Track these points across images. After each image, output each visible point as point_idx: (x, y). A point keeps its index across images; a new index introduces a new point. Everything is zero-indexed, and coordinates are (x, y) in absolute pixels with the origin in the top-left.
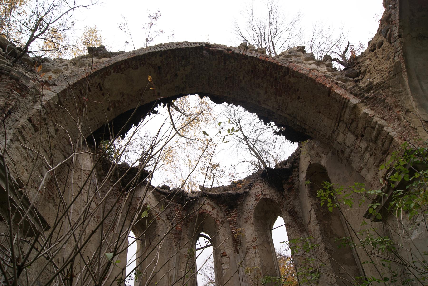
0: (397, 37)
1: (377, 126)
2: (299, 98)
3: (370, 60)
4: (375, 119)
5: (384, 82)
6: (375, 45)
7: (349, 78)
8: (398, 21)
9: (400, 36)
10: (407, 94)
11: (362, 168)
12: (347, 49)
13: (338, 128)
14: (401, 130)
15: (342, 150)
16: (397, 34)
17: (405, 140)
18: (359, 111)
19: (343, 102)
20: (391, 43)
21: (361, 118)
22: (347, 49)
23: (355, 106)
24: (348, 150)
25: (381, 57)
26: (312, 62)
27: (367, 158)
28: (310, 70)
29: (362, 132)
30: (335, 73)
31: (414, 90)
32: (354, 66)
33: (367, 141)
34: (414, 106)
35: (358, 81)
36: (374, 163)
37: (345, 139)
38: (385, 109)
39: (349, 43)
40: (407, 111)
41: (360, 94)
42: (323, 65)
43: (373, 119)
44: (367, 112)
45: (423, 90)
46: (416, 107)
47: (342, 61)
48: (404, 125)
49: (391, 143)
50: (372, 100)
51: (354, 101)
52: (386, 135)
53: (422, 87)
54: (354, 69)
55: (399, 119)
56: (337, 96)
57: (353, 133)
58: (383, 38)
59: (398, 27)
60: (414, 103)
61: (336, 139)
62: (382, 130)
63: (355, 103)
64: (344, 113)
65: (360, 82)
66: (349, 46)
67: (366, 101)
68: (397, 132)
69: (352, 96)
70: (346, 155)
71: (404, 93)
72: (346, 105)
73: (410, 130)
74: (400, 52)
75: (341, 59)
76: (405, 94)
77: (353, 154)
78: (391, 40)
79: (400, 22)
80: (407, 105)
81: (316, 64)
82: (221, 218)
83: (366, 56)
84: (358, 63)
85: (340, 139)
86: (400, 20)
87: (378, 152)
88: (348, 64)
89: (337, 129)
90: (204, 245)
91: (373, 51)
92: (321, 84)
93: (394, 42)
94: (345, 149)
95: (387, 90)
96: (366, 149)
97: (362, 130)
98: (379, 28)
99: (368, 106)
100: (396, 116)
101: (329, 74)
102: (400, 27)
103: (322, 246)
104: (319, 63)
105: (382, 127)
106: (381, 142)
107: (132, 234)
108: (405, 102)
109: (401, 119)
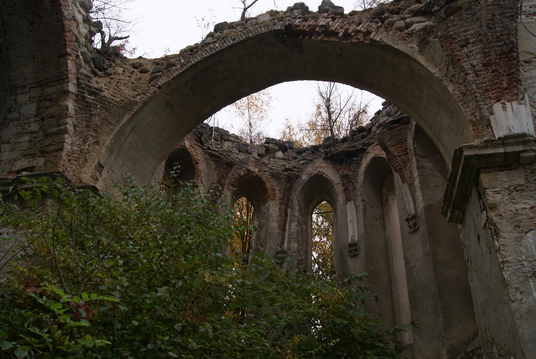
0: (157, 86)
1: (63, 127)
2: (32, 23)
3: (124, 71)
4: (69, 121)
5: (110, 102)
6: (142, 66)
7: (92, 64)
8: (172, 77)
9: (160, 88)
10: (112, 131)
11: (8, 142)
12: (121, 38)
13: (32, 89)
14: (76, 150)
15: (10, 109)
16: (160, 84)
17: (69, 160)
18: (66, 100)
19: (62, 77)
20: (150, 83)
21: (60, 105)
22: (121, 38)
23: (67, 92)
24: (16, 115)
25: (133, 80)
26: (84, 13)
27: (24, 140)
28: (73, 17)
29: (46, 116)
30: (89, 44)
31: (120, 133)
32: (110, 56)
33: (41, 127)
34: (106, 145)
35: (96, 74)
36: (24, 150)
37: (25, 104)
38: (84, 122)
39: (128, 37)
40: (97, 143)
41: (83, 88)
42: (88, 26)
43: (67, 118)
44: (70, 108)
45: (125, 140)
46: (107, 146)
47: (106, 42)
48: (82, 150)
49: (57, 151)
50: (85, 104)
51: (72, 88)
52: (60, 141)
53: (127, 137)
54: (104, 61)
55: (85, 141)
56: (64, 66)
57: (38, 108)
58: (151, 70)
59: (167, 80)
60: (109, 141)
61: (17, 95)
62: (62, 134)
63: (70, 90)
64: (53, 86)
65: (95, 76)
66: (125, 39)
67: (80, 99)
68: (71, 149)
69: (75, 82)
70: (9, 116)
71: (112, 127)
72: (62, 82)
73: (81, 158)
74: (146, 97)
75: (107, 39)
76: (111, 129)
77: (16, 123)
78: (152, 81)
79: (172, 79)
80: (103, 138)
81: (84, 18)
83: (125, 64)
84: (114, 61)
85: (21, 99)
86: (174, 78)
87: (38, 146)
88: (107, 51)
89: (30, 88)
91: (134, 67)
92: (65, 40)
93: (152, 86)
94: (15, 111)
95: (104, 111)
96: (32, 133)
97: (49, 115)
98: (159, 59)
99: (76, 104)
100: (85, 136)
101: (82, 40)
102: (168, 83)
104: (87, 20)
105: (66, 132)
106: (50, 142)
108: (104, 134)
109: (86, 143)
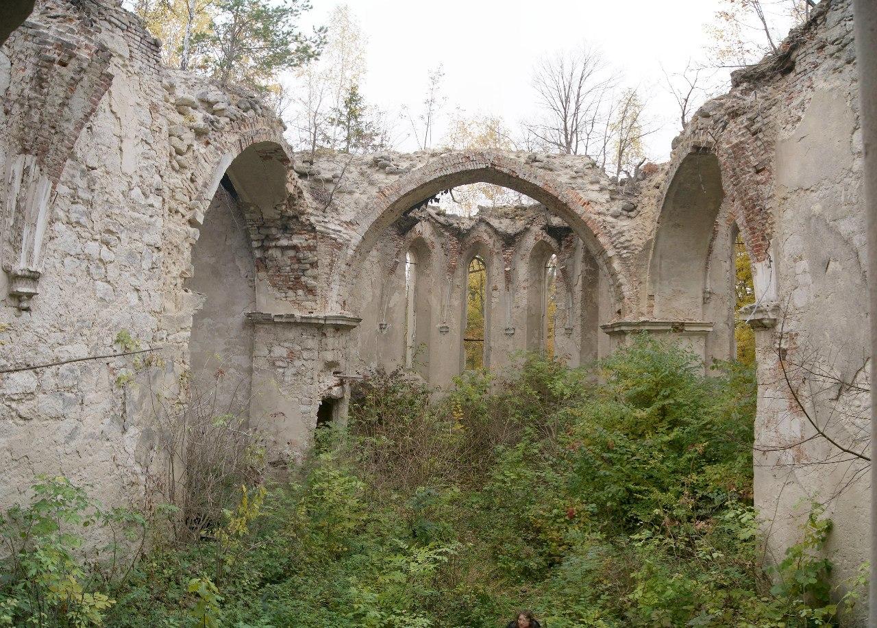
31: (653, 266)
45: (660, 268)
53: (661, 264)
82: (497, 249)
90: (477, 268)
103: (579, 312)
107: (408, 257)
